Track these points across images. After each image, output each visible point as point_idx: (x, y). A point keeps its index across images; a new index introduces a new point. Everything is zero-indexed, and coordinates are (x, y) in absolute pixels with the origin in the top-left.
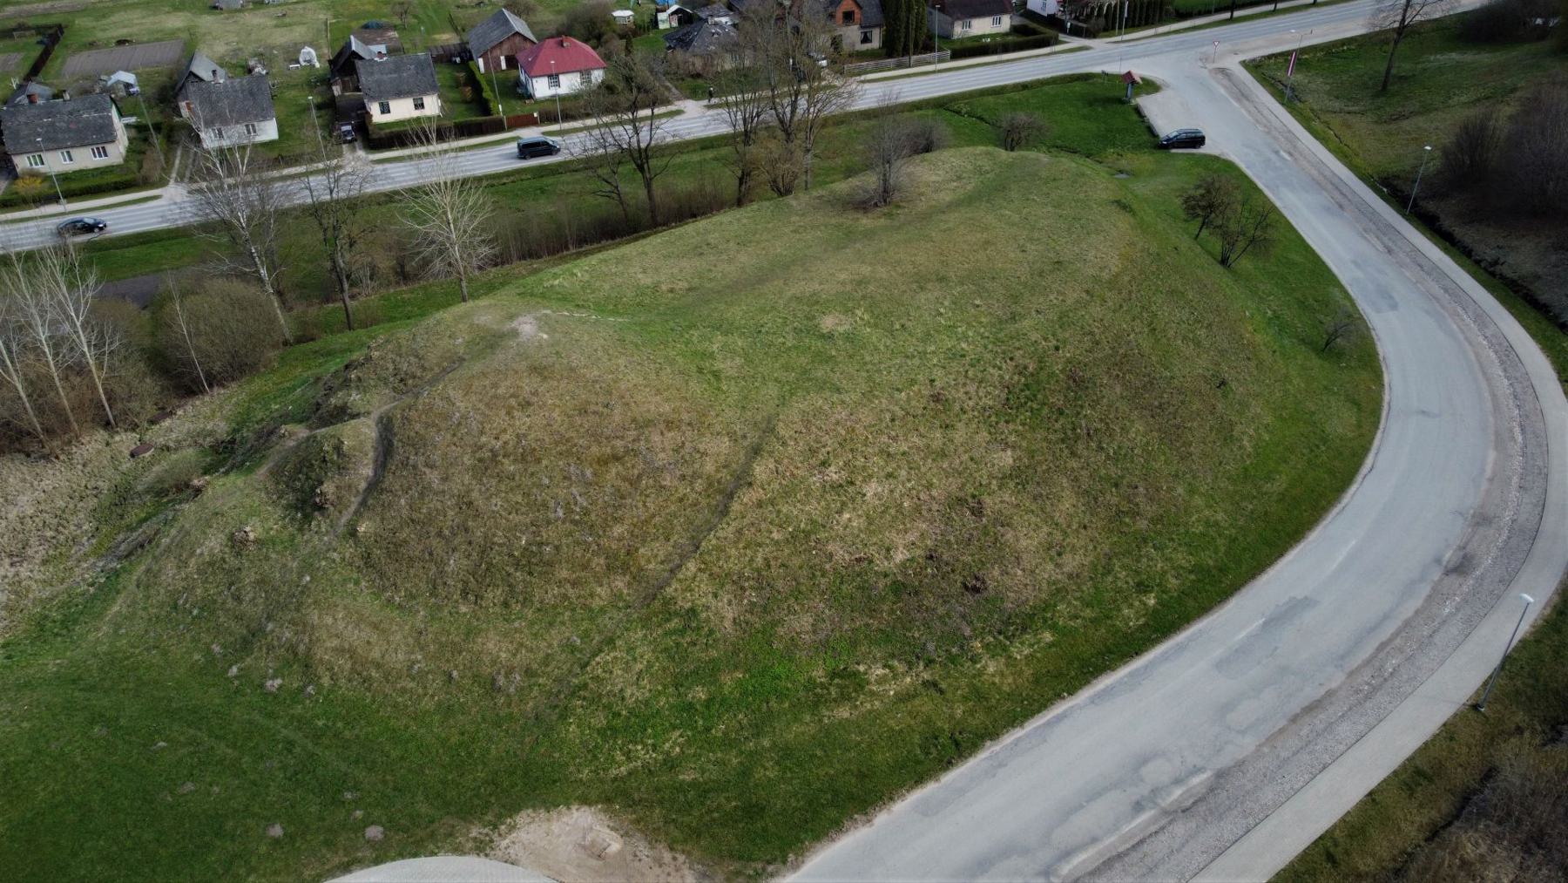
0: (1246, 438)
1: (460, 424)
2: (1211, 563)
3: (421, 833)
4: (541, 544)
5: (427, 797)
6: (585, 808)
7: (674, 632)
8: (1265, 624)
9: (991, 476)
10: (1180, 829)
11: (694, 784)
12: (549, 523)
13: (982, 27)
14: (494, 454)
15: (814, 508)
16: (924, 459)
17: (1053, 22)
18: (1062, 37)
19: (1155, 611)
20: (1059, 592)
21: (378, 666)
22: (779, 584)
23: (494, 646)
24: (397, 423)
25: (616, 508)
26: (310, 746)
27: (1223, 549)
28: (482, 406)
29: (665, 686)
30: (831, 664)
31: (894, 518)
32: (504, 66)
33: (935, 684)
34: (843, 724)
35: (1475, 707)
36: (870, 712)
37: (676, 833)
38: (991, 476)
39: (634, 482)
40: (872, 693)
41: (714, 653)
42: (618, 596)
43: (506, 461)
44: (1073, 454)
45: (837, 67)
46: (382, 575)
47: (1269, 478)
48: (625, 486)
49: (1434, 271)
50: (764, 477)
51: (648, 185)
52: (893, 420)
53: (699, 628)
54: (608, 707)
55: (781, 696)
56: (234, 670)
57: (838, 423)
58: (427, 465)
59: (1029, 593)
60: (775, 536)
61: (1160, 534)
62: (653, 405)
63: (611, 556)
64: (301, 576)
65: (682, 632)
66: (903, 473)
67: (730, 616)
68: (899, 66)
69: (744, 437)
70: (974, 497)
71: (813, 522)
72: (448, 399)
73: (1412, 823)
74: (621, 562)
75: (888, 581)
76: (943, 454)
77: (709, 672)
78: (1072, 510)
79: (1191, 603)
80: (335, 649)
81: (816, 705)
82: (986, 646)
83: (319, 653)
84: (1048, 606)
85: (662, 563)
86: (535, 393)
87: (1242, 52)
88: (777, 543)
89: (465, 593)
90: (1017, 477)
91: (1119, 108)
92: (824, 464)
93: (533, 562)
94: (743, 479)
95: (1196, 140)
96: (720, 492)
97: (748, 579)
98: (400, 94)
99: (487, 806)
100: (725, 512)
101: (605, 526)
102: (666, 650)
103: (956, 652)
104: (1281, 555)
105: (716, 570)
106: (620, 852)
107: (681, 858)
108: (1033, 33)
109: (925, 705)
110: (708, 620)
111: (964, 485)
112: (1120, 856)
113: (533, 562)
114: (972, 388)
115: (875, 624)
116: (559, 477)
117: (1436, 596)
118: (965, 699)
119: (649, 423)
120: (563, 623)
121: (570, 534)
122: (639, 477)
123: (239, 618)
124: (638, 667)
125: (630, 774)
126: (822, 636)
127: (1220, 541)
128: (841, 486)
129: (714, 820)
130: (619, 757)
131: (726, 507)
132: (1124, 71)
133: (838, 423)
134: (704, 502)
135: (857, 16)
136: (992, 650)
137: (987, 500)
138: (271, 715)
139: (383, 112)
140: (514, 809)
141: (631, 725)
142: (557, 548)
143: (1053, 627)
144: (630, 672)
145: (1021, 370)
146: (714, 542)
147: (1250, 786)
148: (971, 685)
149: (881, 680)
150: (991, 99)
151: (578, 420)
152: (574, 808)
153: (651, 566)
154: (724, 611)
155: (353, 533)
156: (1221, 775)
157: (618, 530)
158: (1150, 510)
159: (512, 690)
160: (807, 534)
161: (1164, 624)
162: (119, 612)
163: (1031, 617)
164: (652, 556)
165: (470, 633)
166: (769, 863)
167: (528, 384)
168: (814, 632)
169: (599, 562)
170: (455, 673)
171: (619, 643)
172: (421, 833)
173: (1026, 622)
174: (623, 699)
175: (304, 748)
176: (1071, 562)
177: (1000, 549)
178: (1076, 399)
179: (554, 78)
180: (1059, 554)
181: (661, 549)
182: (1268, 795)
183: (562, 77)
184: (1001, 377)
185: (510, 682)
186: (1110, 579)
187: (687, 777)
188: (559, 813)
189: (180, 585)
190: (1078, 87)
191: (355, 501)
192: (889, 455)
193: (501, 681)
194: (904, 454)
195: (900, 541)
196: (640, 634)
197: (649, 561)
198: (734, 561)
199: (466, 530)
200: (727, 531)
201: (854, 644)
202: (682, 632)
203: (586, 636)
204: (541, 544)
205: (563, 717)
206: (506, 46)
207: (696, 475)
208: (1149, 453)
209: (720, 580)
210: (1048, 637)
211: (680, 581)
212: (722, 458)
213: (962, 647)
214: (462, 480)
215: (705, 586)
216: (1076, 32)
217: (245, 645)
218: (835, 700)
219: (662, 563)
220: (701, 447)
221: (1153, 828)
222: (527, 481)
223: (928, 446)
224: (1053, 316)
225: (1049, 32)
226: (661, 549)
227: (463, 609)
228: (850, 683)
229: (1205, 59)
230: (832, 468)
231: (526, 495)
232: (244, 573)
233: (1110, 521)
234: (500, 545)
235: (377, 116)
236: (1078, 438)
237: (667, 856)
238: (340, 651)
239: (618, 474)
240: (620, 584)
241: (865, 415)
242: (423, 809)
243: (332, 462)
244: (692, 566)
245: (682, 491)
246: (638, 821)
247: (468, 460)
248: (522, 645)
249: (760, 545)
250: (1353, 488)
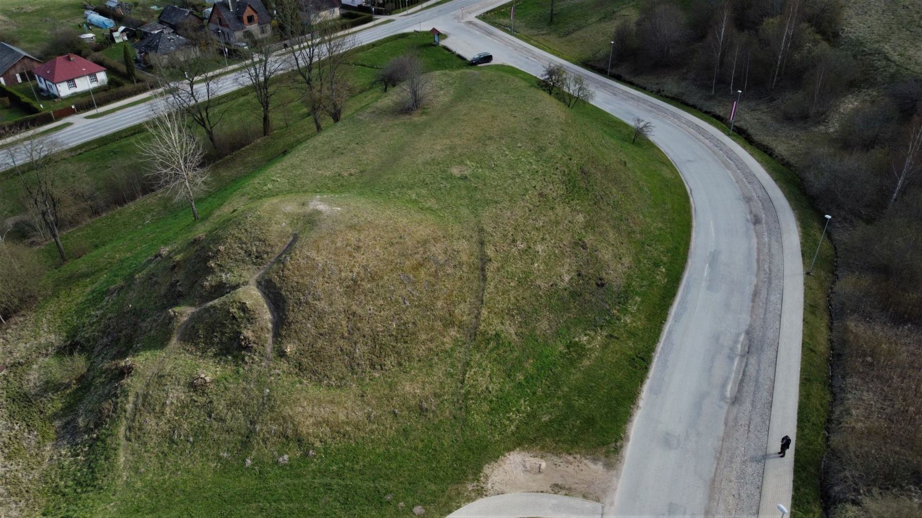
1: (324, 270)
3: (444, 500)
5: (429, 480)
6: (512, 453)
8: (710, 266)
10: (753, 360)
11: (551, 421)
14: (355, 281)
21: (348, 423)
22: (526, 308)
23: (410, 388)
24: (276, 279)
26: (341, 482)
30: (564, 341)
32: (20, 80)
33: (611, 336)
35: (808, 274)
37: (565, 446)
39: (435, 275)
41: (516, 354)
42: (456, 340)
46: (314, 372)
49: (638, 99)
54: (485, 398)
56: (249, 461)
58: (315, 299)
62: (423, 232)
64: (262, 391)
67: (513, 332)
72: (307, 257)
73: (822, 324)
74: (449, 322)
76: (558, 223)
77: (518, 365)
80: (314, 424)
81: (572, 364)
83: (303, 430)
84: (629, 285)
85: (469, 315)
87: (473, 12)
89: (373, 366)
90: (589, 226)
92: (514, 241)
93: (405, 335)
94: (485, 260)
95: (488, 58)
96: (477, 269)
100: (484, 279)
101: (433, 304)
102: (495, 360)
107: (578, 456)
108: (356, 17)
109: (615, 346)
110: (506, 338)
112: (742, 381)
113: (405, 335)
117: (759, 235)
118: (629, 338)
121: (417, 314)
122: (436, 271)
123: (229, 431)
124: (488, 372)
125: (518, 428)
132: (429, 29)
134: (472, 276)
135: (256, 18)
136: (625, 311)
138: (298, 476)
140: (478, 469)
141: (501, 404)
142: (414, 323)
143: (637, 294)
144: (485, 378)
147: (761, 334)
149: (589, 342)
151: (391, 249)
153: (465, 318)
154: (510, 330)
156: (748, 333)
157: (439, 304)
162: (127, 460)
164: (462, 311)
165: (392, 386)
166: (616, 442)
167: (352, 236)
169: (438, 324)
171: (472, 363)
172: (444, 500)
174: (490, 392)
175: (338, 485)
179: (71, 81)
182: (770, 334)
183: (76, 81)
187: (546, 418)
189: (166, 428)
191: (269, 336)
193: (425, 405)
196: (478, 356)
197: (462, 316)
199: (358, 329)
200: (491, 287)
201: (568, 329)
203: (453, 365)
204: (405, 324)
206: (18, 67)
209: (500, 314)
211: (484, 321)
214: (341, 302)
216: (379, 13)
217: (246, 443)
219: (469, 315)
221: (744, 364)
222: (382, 291)
225: (368, 15)
228: (576, 351)
229: (457, 18)
231: (385, 299)
232: (215, 403)
234: (382, 332)
237: (570, 458)
238: (317, 424)
240: (454, 333)
241: (519, 212)
243: (240, 317)
245: (458, 274)
248: (424, 382)
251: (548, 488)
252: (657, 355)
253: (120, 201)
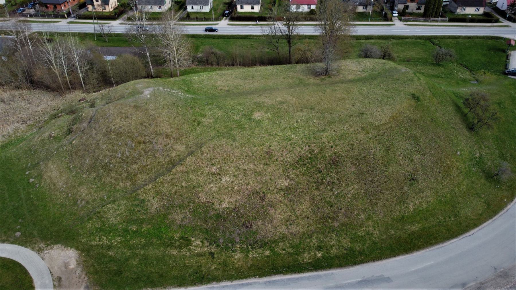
0: (412, 204)
2: (358, 249)
4: (110, 163)
7: (135, 205)
8: (361, 281)
9: (276, 187)
11: (110, 257)
12: (115, 157)
13: (470, 11)
15: (202, 179)
16: (251, 174)
17: (503, 13)
18: (501, 19)
19: (319, 259)
20: (283, 238)
25: (137, 159)
27: (367, 245)
28: (115, 114)
29: (124, 222)
31: (229, 192)
34: (171, 256)
36: (183, 255)
38: (276, 187)
39: (146, 152)
40: (190, 249)
42: (125, 187)
43: (113, 134)
44: (318, 189)
45: (400, 17)
47: (412, 223)
48: (143, 152)
50: (189, 163)
51: (290, 47)
52: (246, 156)
53: (143, 207)
54: (103, 222)
55: (159, 238)
57: (225, 152)
59: (270, 235)
60: (183, 184)
61: (343, 230)
63: (129, 174)
65: (137, 206)
66: (241, 176)
67: (156, 206)
68: (425, 21)
69: (190, 147)
70: (264, 193)
71: (199, 184)
74: (131, 177)
75: (216, 212)
77: (140, 222)
78: (305, 210)
79: (337, 261)
80: (48, 176)
82: (241, 248)
84: (276, 242)
85: (143, 181)
86: (131, 115)
88: (182, 187)
89: (87, 171)
91: (501, 54)
97: (166, 196)
98: (247, 3)
99: (51, 239)
103: (230, 245)
104: (394, 256)
105: (158, 189)
106: (72, 269)
107: (86, 278)
111: (262, 187)
114: (285, 153)
115: (205, 226)
116: (124, 144)
119: (161, 134)
120: (106, 191)
122: (149, 151)
126: (184, 223)
127: (368, 242)
128: (215, 174)
129: (105, 271)
130: (97, 238)
131: (172, 169)
133: (225, 152)
137: (269, 196)
139: (241, 8)
140: (56, 243)
141: (105, 229)
142: (115, 166)
143: (272, 251)
144: (114, 215)
145: (311, 151)
146: (161, 180)
148: (225, 261)
149: (197, 246)
150: (450, 40)
152: (72, 249)
154: (154, 204)
155: (71, 143)
157: (135, 166)
158: (343, 220)
159: (80, 206)
160: (195, 187)
161: (317, 265)
163: (266, 244)
164: (141, 178)
168: (181, 221)
169: (125, 175)
170: (70, 195)
171: (117, 203)
173: (263, 245)
174: (109, 221)
176: (293, 229)
177: (266, 215)
178: (330, 168)
180: (291, 225)
181: (145, 177)
184: (300, 152)
185: (81, 203)
186: (308, 240)
188: (67, 249)
190: (490, 42)
192: (239, 168)
194: (244, 170)
195: (227, 200)
197: (139, 180)
198: (165, 189)
199: (94, 152)
200: (167, 178)
201: (194, 230)
202: (137, 206)
203: (109, 197)
204: (110, 163)
205: (89, 220)
207: (168, 156)
208: (354, 198)
210: (267, 253)
211: (144, 189)
212: (179, 153)
213: (233, 245)
215: (152, 193)
218: (175, 247)
219: (143, 181)
220: (174, 147)
223: (255, 170)
224: (339, 134)
226: (145, 177)
227: (84, 176)
228: (186, 242)
230: (215, 167)
233: (321, 219)
235: (239, 10)
236: (323, 183)
237: (84, 276)
239: (142, 148)
241: (237, 152)
242: (35, 233)
244: (151, 186)
246: (85, 261)
247: (104, 130)
248: (90, 193)
249: (176, 186)
250: (454, 240)
251: (56, 276)
252: (216, 286)
253: (342, 83)
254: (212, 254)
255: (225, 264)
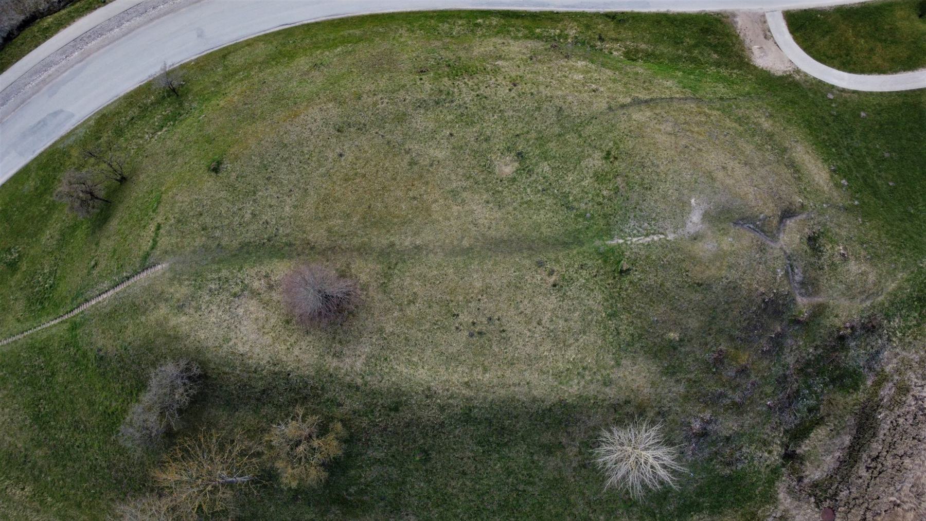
82: (566, 39)
140: (781, 78)
254: (601, 39)
255: (588, 27)
